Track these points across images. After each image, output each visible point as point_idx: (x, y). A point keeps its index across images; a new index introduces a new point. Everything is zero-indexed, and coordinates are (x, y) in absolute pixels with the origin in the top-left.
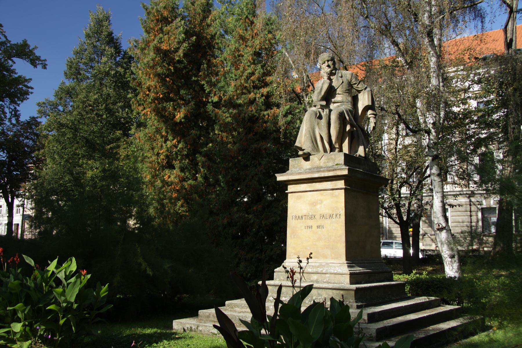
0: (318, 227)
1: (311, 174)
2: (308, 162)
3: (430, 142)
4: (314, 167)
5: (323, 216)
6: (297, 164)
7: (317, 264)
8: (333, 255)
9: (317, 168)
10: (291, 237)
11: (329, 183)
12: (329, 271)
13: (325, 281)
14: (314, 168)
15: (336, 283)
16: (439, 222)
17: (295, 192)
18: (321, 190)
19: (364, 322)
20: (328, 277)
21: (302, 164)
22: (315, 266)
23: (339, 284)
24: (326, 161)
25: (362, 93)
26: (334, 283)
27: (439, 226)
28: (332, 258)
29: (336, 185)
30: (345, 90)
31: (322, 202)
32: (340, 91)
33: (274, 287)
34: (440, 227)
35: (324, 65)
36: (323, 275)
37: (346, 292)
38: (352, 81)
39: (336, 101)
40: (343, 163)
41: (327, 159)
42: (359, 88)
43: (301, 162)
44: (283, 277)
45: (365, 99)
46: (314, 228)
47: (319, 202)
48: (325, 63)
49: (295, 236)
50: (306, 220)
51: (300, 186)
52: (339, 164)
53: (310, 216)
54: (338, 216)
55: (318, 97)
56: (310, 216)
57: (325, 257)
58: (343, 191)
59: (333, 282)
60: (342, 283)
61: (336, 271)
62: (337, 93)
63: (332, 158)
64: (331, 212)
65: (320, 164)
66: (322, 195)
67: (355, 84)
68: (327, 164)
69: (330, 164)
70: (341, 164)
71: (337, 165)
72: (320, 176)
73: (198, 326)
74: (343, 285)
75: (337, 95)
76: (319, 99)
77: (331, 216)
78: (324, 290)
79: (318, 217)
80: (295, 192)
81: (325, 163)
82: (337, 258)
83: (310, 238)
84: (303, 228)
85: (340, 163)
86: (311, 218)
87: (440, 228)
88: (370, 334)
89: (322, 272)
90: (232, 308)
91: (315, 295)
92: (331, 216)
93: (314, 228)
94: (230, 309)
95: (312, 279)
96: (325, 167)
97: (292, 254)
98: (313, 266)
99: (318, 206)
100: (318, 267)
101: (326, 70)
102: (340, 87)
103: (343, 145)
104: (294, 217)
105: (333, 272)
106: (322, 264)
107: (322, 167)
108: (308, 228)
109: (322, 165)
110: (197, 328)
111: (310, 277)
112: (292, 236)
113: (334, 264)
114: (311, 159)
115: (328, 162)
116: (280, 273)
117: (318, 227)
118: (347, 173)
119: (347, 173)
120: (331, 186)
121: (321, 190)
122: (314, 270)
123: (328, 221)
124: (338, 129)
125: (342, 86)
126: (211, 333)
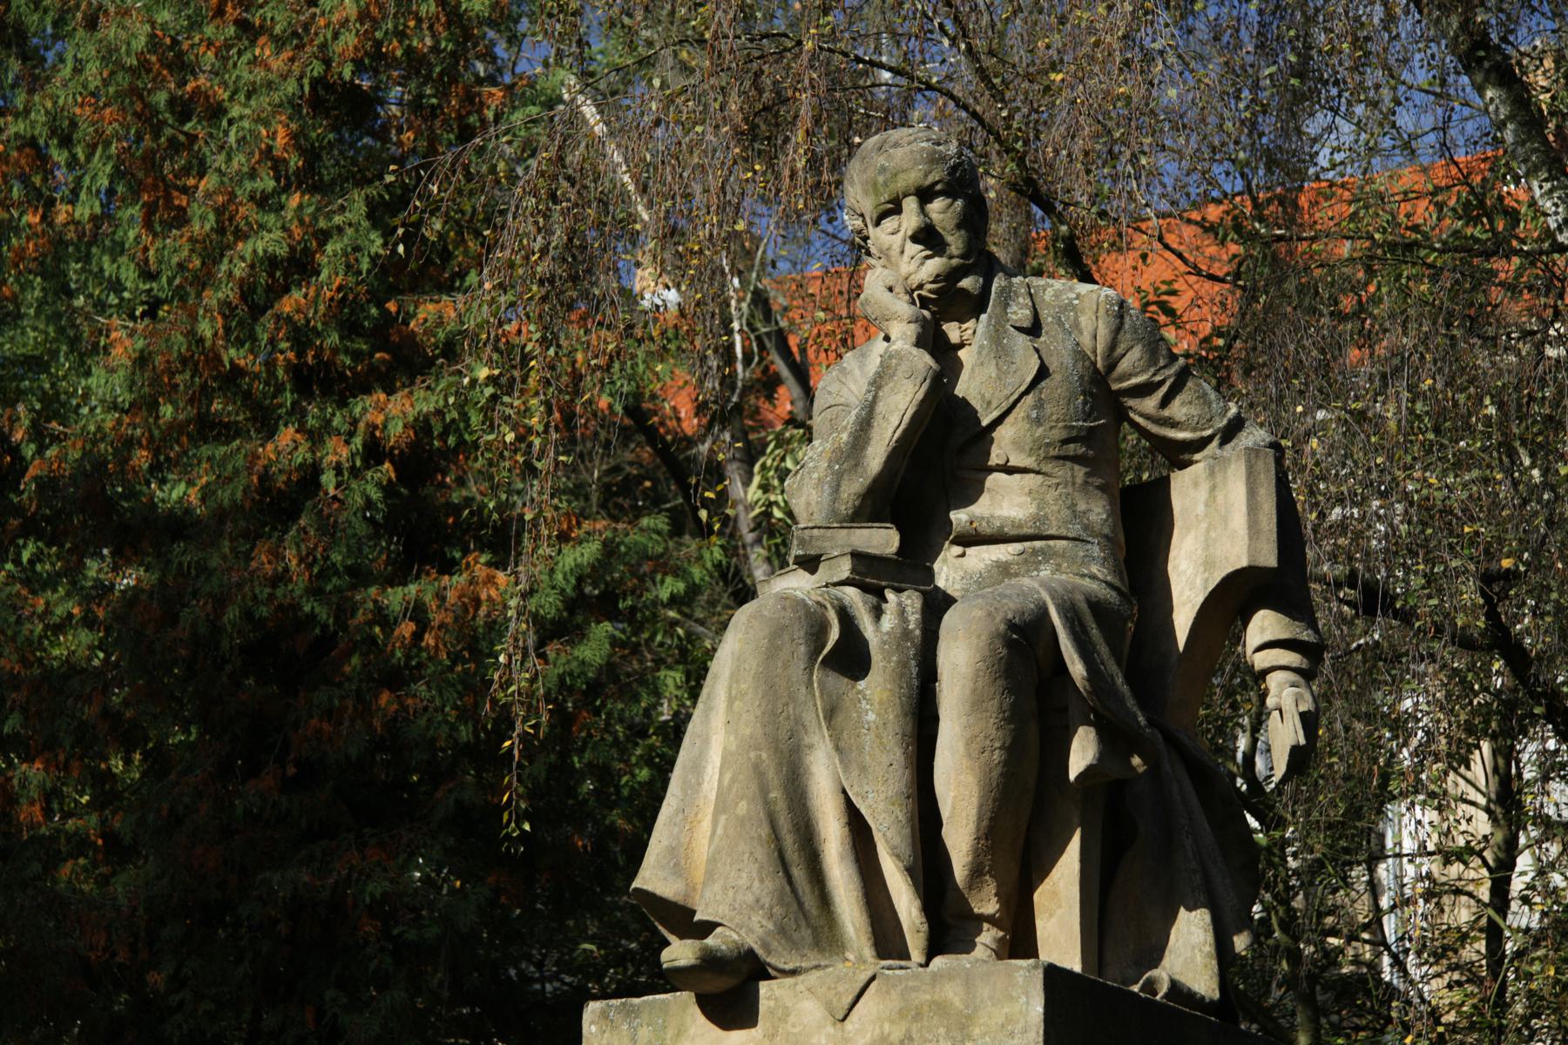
2: (737, 1036)
25: (1198, 469)
30: (1058, 434)
32: (1017, 444)
35: (889, 223)
38: (1124, 365)
41: (902, 1014)
42: (1173, 424)
55: (836, 489)
63: (941, 1008)
102: (1019, 412)
114: (764, 1005)
124: (997, 756)
125: (1039, 405)
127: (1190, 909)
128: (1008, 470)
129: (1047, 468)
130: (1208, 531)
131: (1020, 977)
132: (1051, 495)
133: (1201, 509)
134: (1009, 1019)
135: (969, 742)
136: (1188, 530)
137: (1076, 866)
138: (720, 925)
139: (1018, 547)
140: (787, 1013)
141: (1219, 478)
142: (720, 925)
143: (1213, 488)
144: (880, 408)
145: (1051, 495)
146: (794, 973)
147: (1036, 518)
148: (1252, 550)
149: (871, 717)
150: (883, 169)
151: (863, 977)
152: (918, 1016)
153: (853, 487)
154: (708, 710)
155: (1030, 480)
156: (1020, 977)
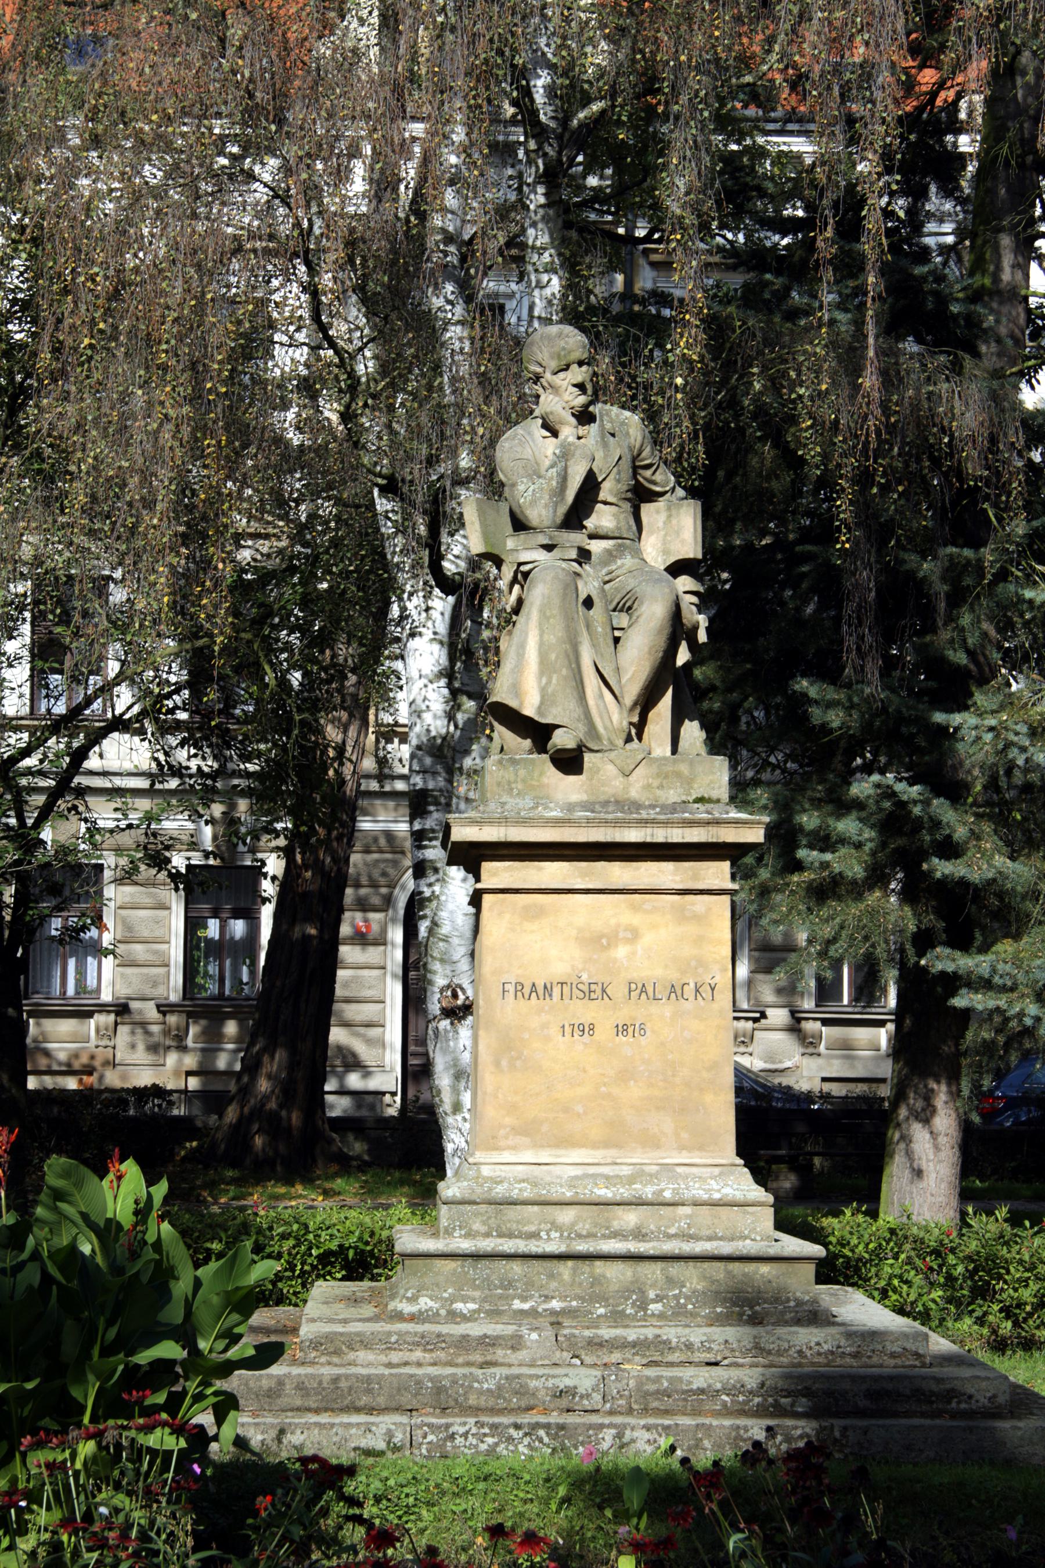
0: (622, 1029)
1: (610, 830)
2: (572, 778)
3: (479, 633)
4: (602, 798)
5: (641, 990)
6: (524, 781)
7: (626, 1171)
8: (685, 1135)
9: (620, 804)
10: (497, 1064)
11: (668, 866)
12: (687, 1195)
13: (672, 1231)
14: (606, 803)
15: (721, 1239)
16: (456, 981)
17: (517, 891)
18: (635, 891)
19: (917, 1363)
20: (687, 1216)
21: (545, 780)
22: (617, 1176)
23: (732, 1240)
24: (656, 783)
25: (661, 504)
26: (710, 1239)
27: (455, 996)
28: (682, 1148)
29: (695, 877)
30: (625, 488)
31: (634, 935)
32: (611, 491)
33: (470, 1260)
34: (459, 1002)
35: (562, 375)
36: (664, 1211)
37: (783, 1266)
38: (644, 454)
39: (601, 532)
40: (725, 796)
41: (658, 775)
42: (654, 483)
43: (541, 774)
44: (484, 1223)
45: (678, 533)
46: (604, 1032)
47: (621, 935)
48: (567, 368)
49: (518, 1063)
50: (567, 1001)
51: (540, 869)
52: (709, 801)
53: (585, 988)
54: (706, 991)
55: (555, 511)
56: (585, 988)
57: (652, 1142)
58: (726, 899)
59: (708, 1233)
60: (746, 1238)
61: (717, 1196)
62: (602, 496)
63: (678, 775)
64: (674, 976)
65: (626, 789)
66: (635, 908)
67: (647, 467)
68: (659, 792)
69: (673, 795)
70: (718, 801)
71: (700, 800)
72: (649, 840)
73: (282, 1432)
74: (748, 1241)
75: (599, 507)
76: (559, 519)
77: (675, 991)
78: (691, 1264)
79: (617, 991)
80: (517, 891)
81: (648, 787)
82: (701, 1148)
83: (585, 1071)
84: (554, 1031)
85: (714, 794)
86: (588, 994)
87: (459, 1008)
88: (988, 1395)
89: (660, 1199)
90: (337, 1352)
91: (653, 1286)
92: (675, 991)
93: (604, 1032)
94: (323, 1359)
95: (616, 1225)
96: (653, 807)
97: (502, 1132)
98: (607, 1177)
99: (621, 952)
100: (631, 1180)
101: (567, 397)
102: (612, 476)
103: (651, 715)
104: (510, 988)
105: (706, 1197)
106: (647, 1168)
107: (637, 806)
108: (577, 1033)
109: (634, 793)
110: (279, 1440)
111: (608, 1220)
112: (504, 1063)
113: (694, 1170)
114: (586, 765)
115: (661, 787)
116: (468, 1208)
117: (622, 1029)
118: (761, 840)
119: (761, 840)
120: (678, 878)
121: (635, 891)
122: (624, 1192)
123: (665, 1009)
124: (661, 654)
125: (619, 473)
126: (355, 1449)
127: (691, 720)
128: (605, 503)
129: (620, 503)
130: (666, 535)
131: (717, 764)
132: (622, 516)
133: (661, 524)
134: (712, 782)
135: (651, 648)
136: (652, 533)
137: (670, 703)
138: (558, 726)
139: (611, 542)
140: (599, 770)
141: (674, 512)
142: (558, 726)
143: (669, 516)
144: (570, 471)
145: (622, 516)
146: (597, 751)
147: (618, 528)
148: (695, 551)
149: (600, 629)
150: (564, 349)
151: (640, 757)
152: (666, 777)
153: (562, 510)
154: (528, 619)
155: (613, 508)
156: (717, 764)
